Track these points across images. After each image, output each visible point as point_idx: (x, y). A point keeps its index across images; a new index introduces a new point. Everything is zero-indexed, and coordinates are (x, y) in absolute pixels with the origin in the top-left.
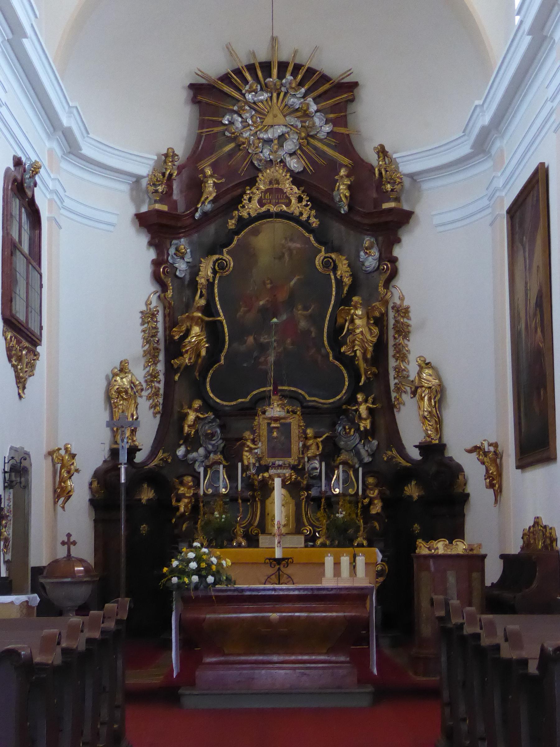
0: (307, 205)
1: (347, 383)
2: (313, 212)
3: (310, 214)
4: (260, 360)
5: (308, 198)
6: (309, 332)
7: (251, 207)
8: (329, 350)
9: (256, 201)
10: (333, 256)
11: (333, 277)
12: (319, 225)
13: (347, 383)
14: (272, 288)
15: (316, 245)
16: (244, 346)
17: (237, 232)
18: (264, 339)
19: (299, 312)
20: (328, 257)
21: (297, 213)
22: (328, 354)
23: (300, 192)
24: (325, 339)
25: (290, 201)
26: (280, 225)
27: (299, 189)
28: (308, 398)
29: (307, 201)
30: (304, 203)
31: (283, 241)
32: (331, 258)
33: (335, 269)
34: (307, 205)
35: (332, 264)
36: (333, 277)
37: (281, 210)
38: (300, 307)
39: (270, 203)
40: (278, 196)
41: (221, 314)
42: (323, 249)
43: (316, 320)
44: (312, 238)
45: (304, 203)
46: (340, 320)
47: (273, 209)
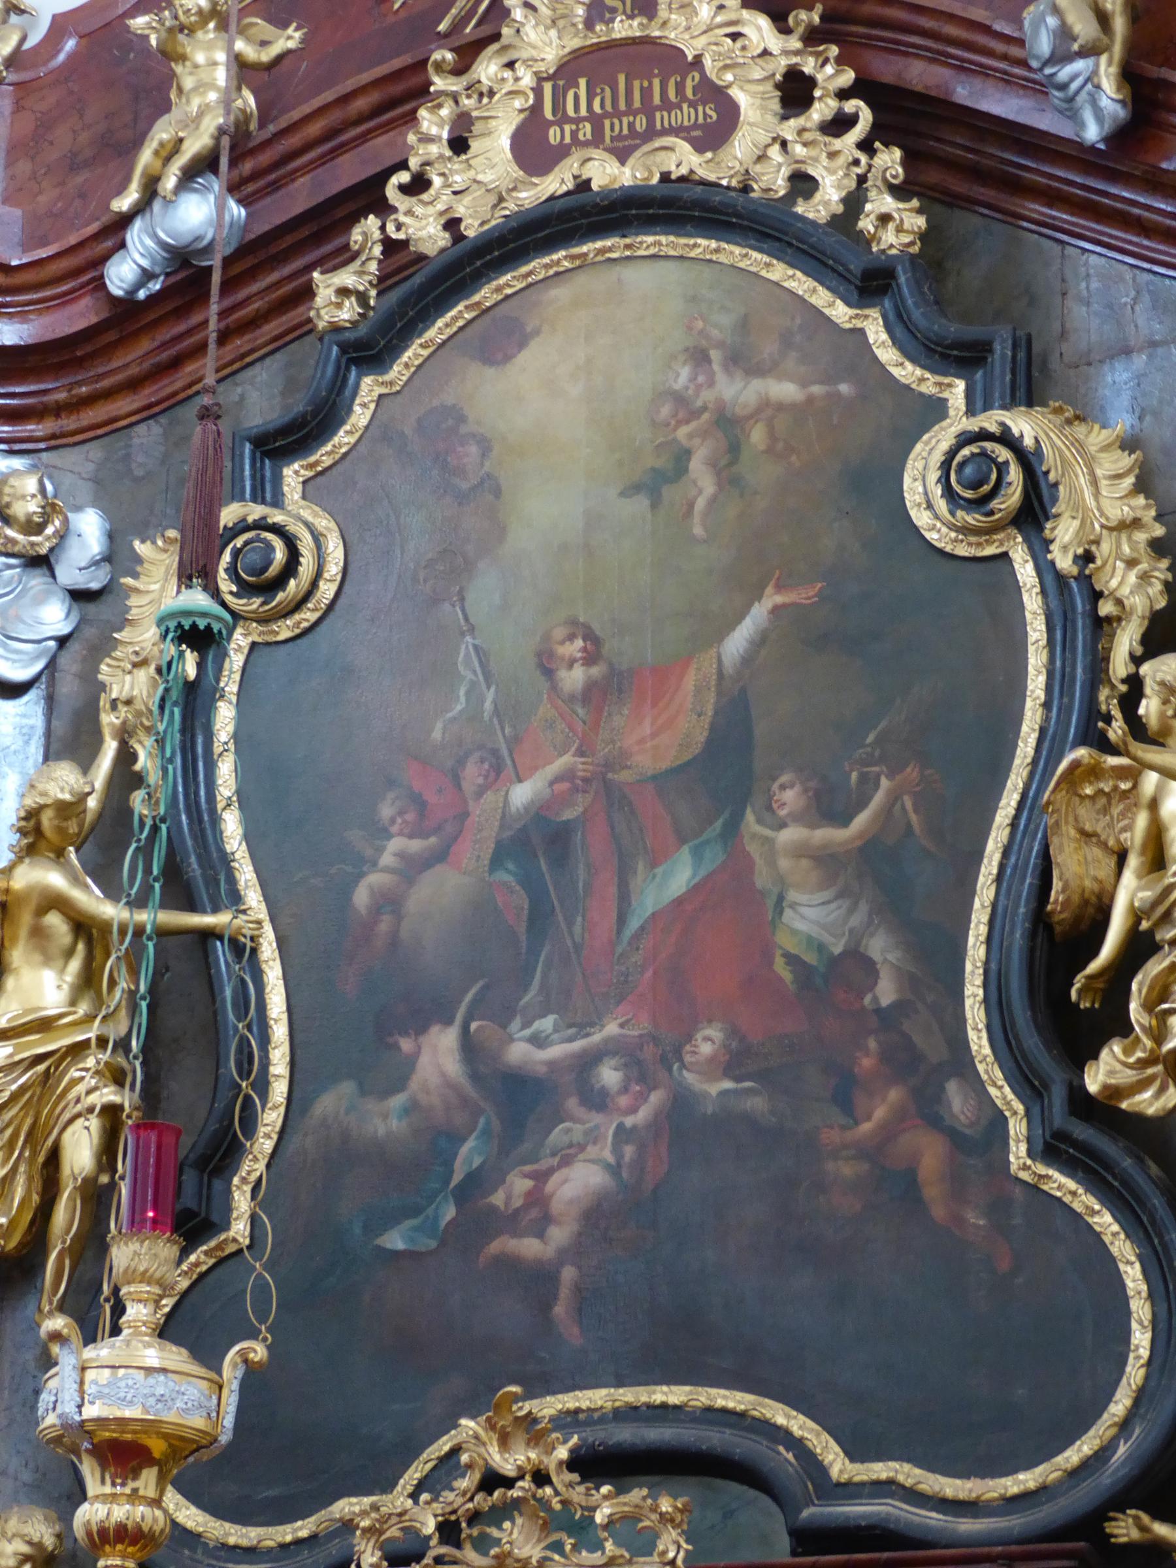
0: (839, 125)
1: (1141, 1339)
2: (890, 160)
3: (862, 179)
4: (498, 1199)
5: (848, 77)
6: (854, 966)
7: (465, 173)
8: (1002, 1093)
9: (505, 142)
10: (1024, 425)
11: (1026, 572)
12: (924, 237)
13: (1141, 1339)
14: (592, 694)
15: (907, 372)
16: (397, 1101)
17: (369, 349)
18: (536, 1045)
19: (785, 835)
20: (984, 435)
21: (774, 179)
22: (999, 1121)
23: (795, 43)
24: (975, 1013)
25: (729, 115)
26: (655, 274)
27: (784, 30)
28: (838, 1464)
29: (843, 95)
30: (822, 110)
31: (683, 376)
32: (1005, 438)
33: (1033, 516)
34: (839, 125)
35: (1015, 474)
36: (1026, 572)
37: (665, 177)
38: (790, 798)
39: (597, 140)
40: (646, 93)
41: (253, 898)
42: (957, 392)
43: (908, 882)
44: (876, 331)
45: (822, 110)
46: (1075, 868)
47: (607, 173)
